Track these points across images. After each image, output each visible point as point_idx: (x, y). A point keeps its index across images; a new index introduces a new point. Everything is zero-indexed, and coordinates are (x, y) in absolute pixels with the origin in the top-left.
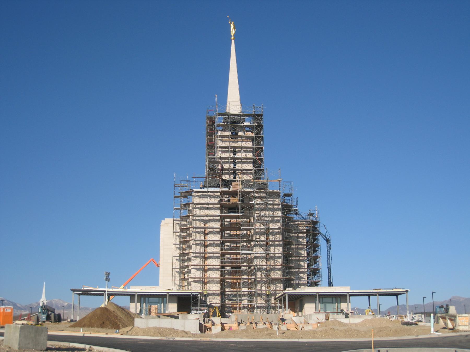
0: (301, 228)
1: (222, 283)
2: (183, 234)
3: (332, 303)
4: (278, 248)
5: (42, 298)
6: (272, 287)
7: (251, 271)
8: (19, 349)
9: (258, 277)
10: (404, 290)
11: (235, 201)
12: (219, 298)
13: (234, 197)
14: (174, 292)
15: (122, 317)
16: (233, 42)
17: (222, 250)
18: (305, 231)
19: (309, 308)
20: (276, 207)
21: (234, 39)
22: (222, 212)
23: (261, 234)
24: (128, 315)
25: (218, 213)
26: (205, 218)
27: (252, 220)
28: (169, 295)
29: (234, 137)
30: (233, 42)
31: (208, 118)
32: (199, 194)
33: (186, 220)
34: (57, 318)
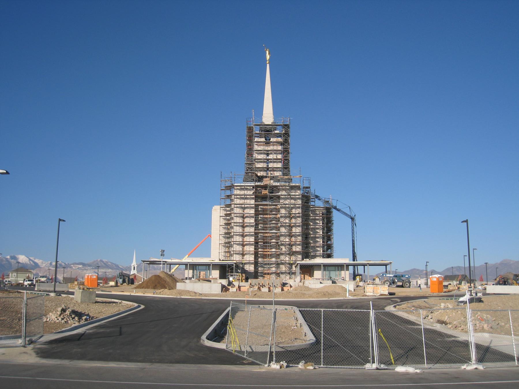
0: (318, 213)
1: (256, 255)
2: (227, 218)
3: (335, 271)
4: (299, 228)
5: (133, 263)
6: (293, 258)
7: (278, 246)
8: (81, 302)
9: (283, 250)
10: (388, 262)
11: (266, 193)
12: (253, 266)
13: (265, 190)
14: (216, 262)
15: (169, 281)
16: (268, 65)
17: (255, 230)
18: (321, 214)
19: (318, 274)
20: (297, 197)
21: (269, 63)
22: (255, 202)
23: (285, 217)
24: (174, 280)
25: (253, 202)
26: (243, 206)
27: (279, 206)
28: (213, 265)
29: (268, 143)
30: (268, 65)
31: (247, 127)
32: (239, 187)
33: (228, 207)
34: (130, 281)
